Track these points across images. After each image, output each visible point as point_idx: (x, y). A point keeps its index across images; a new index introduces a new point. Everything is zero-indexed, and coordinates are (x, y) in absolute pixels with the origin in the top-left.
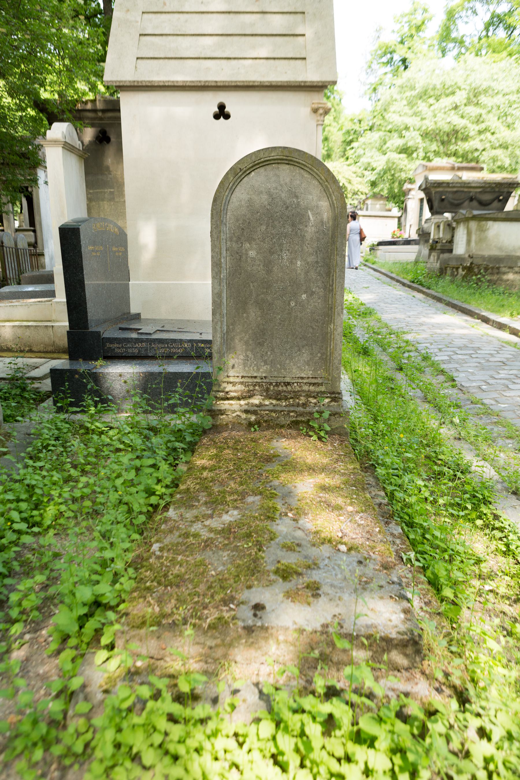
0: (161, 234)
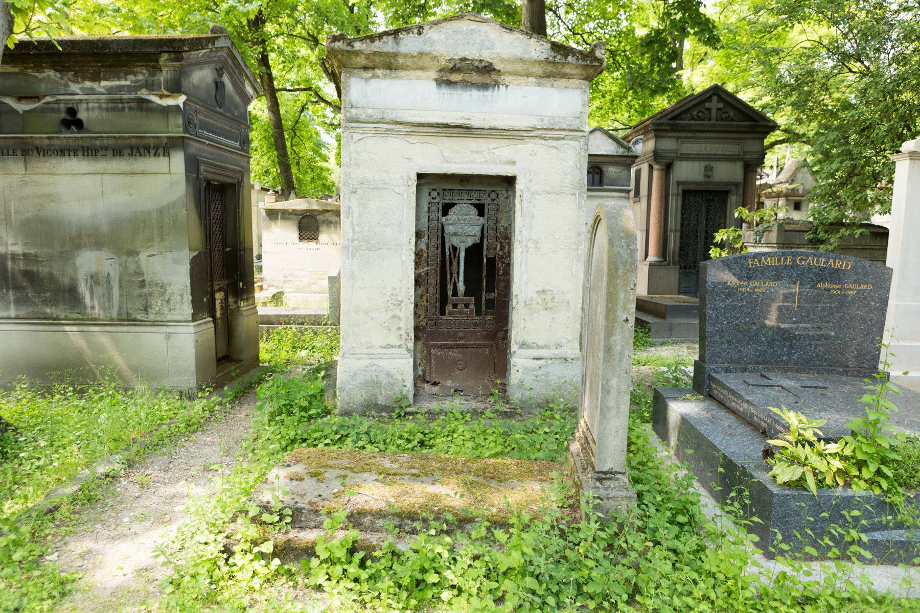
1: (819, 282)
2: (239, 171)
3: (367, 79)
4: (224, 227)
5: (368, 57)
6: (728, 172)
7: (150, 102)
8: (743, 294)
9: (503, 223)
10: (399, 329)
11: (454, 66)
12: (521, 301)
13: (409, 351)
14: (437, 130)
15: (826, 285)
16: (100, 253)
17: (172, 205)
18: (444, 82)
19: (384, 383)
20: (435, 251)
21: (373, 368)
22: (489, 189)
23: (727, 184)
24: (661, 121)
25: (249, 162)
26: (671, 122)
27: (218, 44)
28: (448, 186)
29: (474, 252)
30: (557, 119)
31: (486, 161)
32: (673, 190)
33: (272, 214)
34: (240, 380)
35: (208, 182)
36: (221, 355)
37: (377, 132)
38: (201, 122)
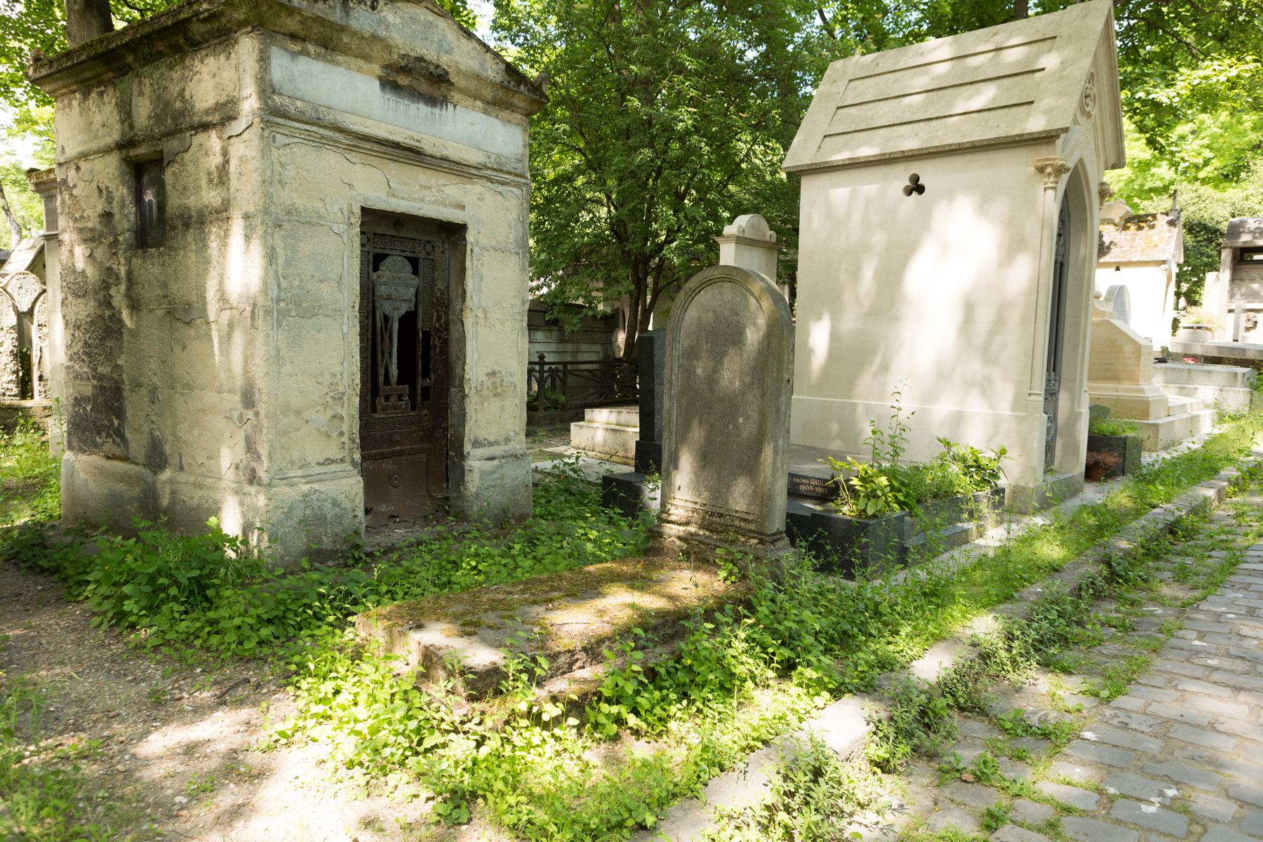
0: (834, 336)
3: (295, 55)
9: (440, 285)
10: (342, 434)
13: (353, 463)
14: (383, 148)
18: (389, 84)
19: (329, 516)
29: (408, 320)
31: (435, 201)
37: (309, 139)
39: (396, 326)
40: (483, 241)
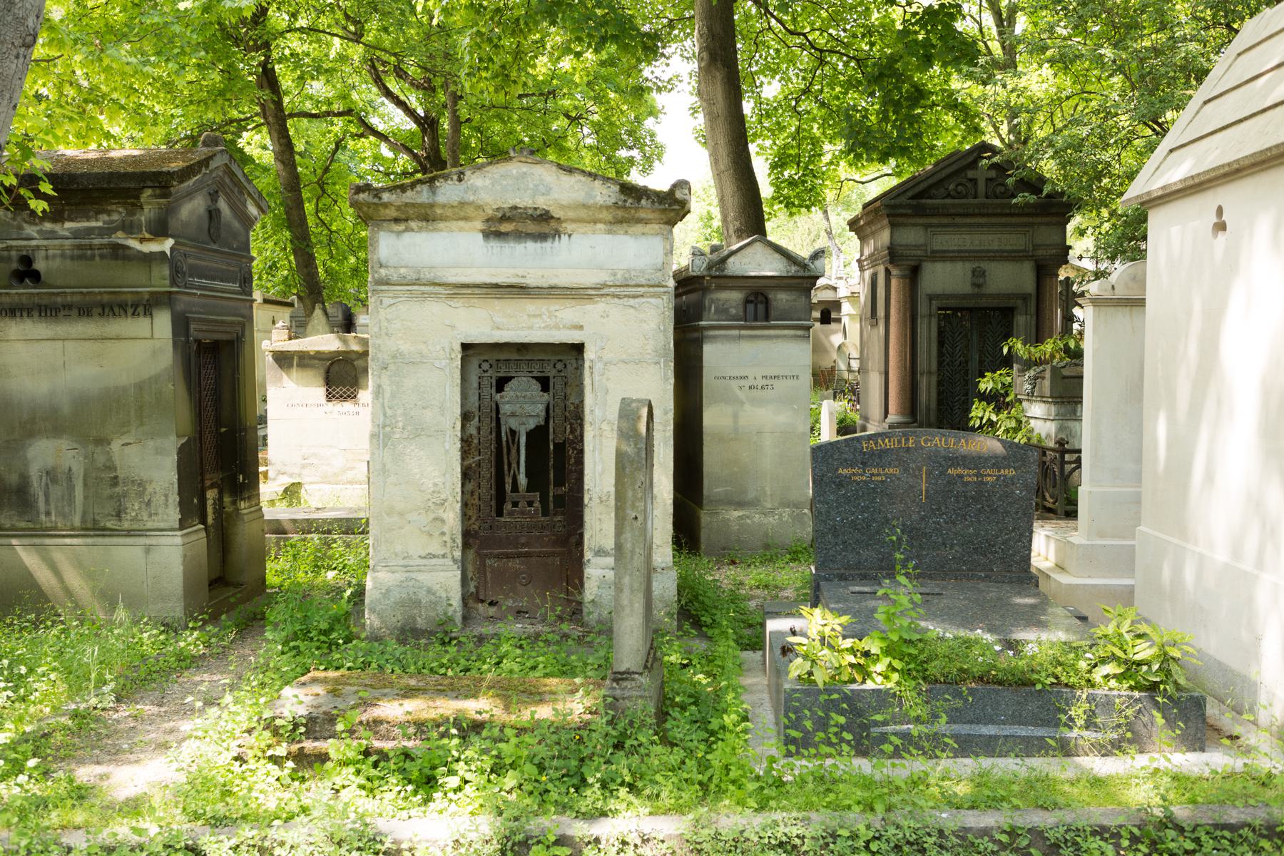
1: (950, 467)
2: (239, 323)
3: (399, 233)
4: (218, 400)
5: (398, 208)
6: (1009, 278)
7: (128, 248)
8: (858, 483)
9: (573, 399)
11: (504, 215)
12: (595, 496)
13: (455, 561)
14: (484, 291)
15: (959, 471)
16: (60, 441)
17: (155, 379)
18: (493, 234)
20: (487, 436)
21: (411, 584)
22: (554, 358)
23: (1009, 296)
24: (898, 201)
25: (251, 307)
26: (914, 202)
27: (213, 165)
28: (503, 356)
29: (538, 436)
30: (633, 273)
32: (922, 308)
33: (283, 360)
34: (241, 607)
35: (198, 342)
36: (213, 577)
37: (412, 296)
38: (191, 267)
39: (523, 440)
40: (608, 356)
